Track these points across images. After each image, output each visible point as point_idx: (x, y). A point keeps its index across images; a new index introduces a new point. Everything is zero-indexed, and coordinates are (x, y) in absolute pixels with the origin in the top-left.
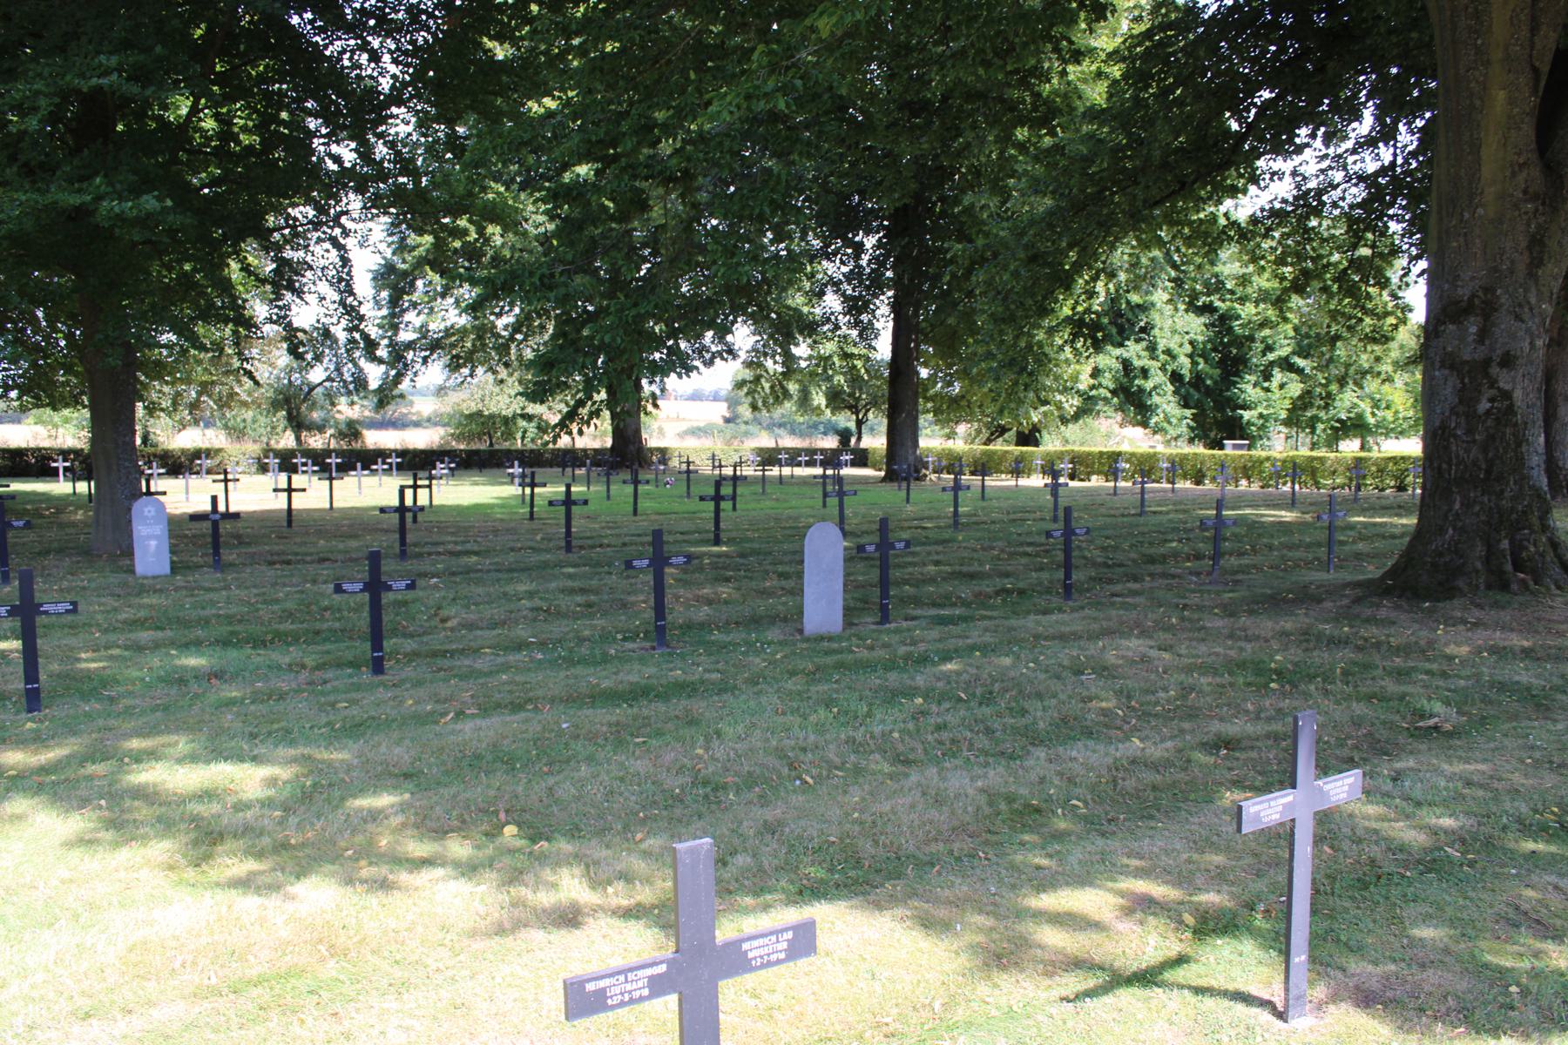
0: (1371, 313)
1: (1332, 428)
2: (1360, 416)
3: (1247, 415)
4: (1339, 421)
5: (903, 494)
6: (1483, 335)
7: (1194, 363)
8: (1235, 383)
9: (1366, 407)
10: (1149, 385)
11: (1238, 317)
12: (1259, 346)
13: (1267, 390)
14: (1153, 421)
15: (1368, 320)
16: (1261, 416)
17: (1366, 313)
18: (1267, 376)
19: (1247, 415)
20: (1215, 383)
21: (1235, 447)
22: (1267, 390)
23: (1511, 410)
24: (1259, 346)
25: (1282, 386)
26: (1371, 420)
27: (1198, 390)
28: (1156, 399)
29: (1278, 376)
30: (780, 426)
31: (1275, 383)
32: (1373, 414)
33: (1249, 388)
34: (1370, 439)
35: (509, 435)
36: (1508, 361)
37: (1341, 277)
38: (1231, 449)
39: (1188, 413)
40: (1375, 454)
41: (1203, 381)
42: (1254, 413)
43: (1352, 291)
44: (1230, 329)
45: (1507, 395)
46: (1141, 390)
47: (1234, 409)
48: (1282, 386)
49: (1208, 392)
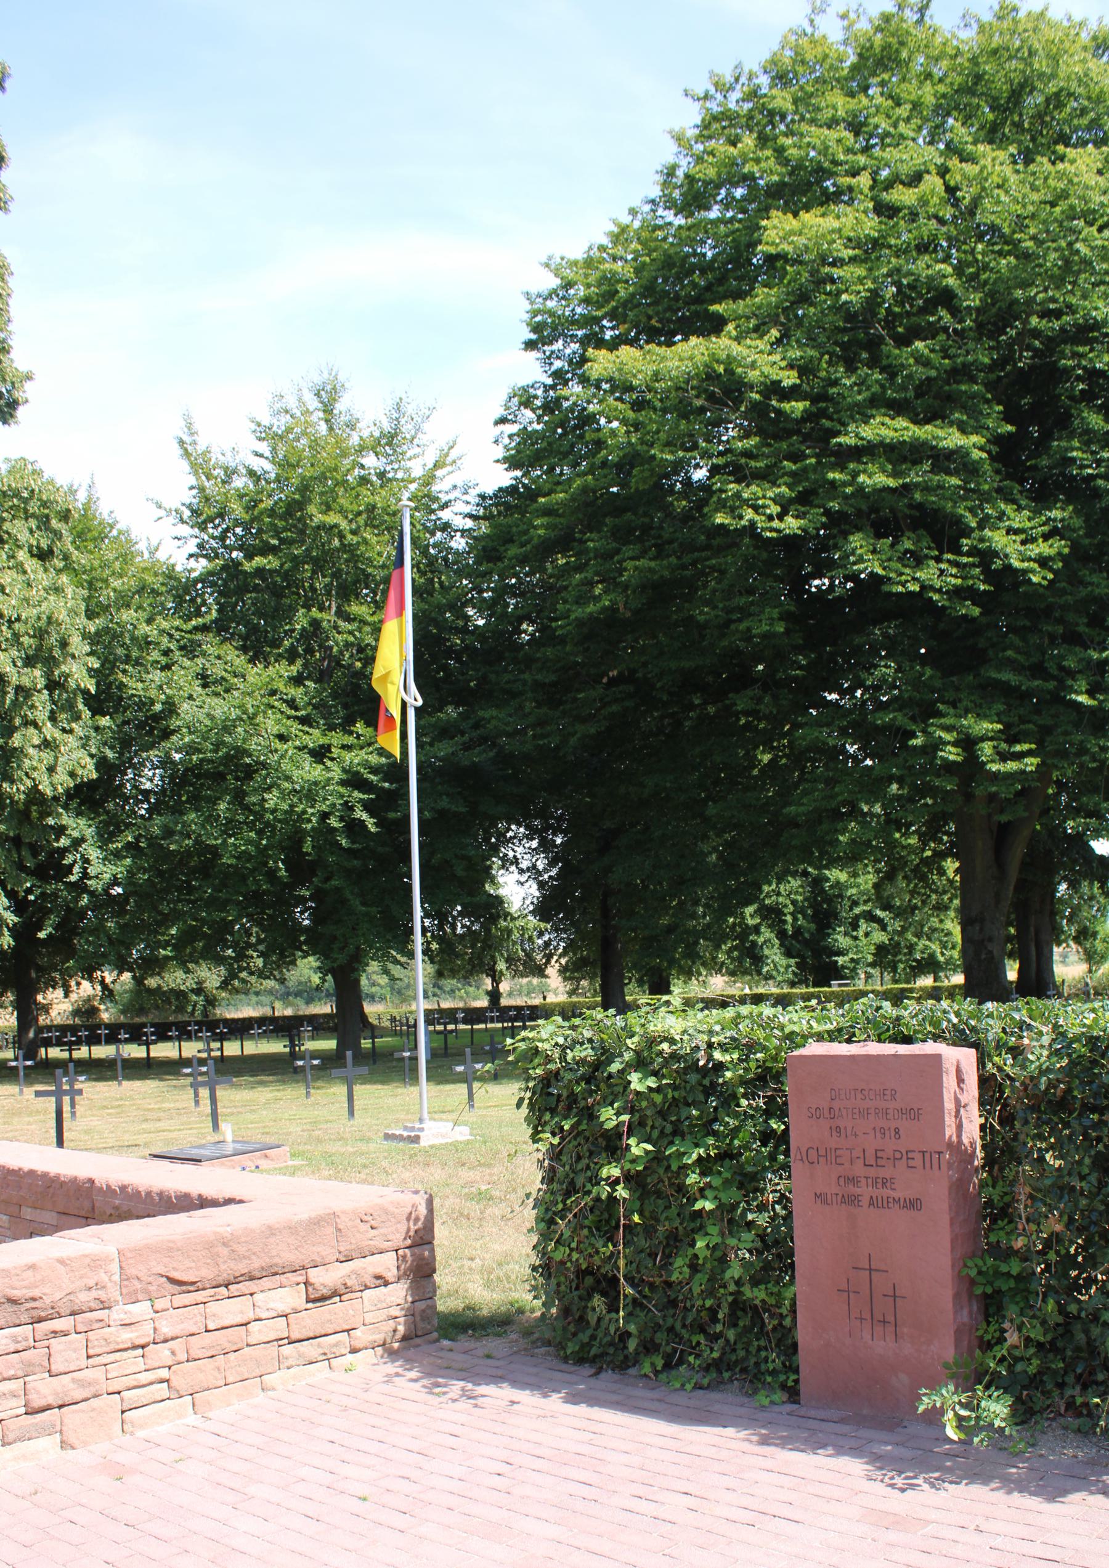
0: (936, 891)
1: (911, 967)
2: (932, 956)
3: (841, 960)
4: (915, 960)
5: (206, 1106)
6: (981, 930)
7: (795, 919)
8: (829, 935)
9: (935, 947)
10: (761, 940)
11: (828, 880)
12: (847, 903)
13: (856, 938)
14: (765, 969)
15: (934, 896)
16: (852, 960)
17: (932, 891)
18: (855, 926)
19: (841, 960)
20: (812, 934)
21: (840, 985)
22: (856, 938)
23: (993, 958)
24: (847, 903)
25: (867, 935)
26: (942, 959)
27: (798, 942)
28: (766, 952)
29: (863, 926)
30: (297, 994)
31: (861, 933)
32: (943, 954)
33: (840, 938)
34: (941, 974)
35: (181, 1009)
36: (990, 939)
37: (916, 870)
38: (835, 986)
39: (792, 961)
40: (946, 983)
41: (802, 934)
42: (846, 958)
43: (923, 878)
44: (823, 890)
45: (991, 952)
46: (754, 944)
47: (829, 956)
48: (867, 935)
49: (806, 943)
